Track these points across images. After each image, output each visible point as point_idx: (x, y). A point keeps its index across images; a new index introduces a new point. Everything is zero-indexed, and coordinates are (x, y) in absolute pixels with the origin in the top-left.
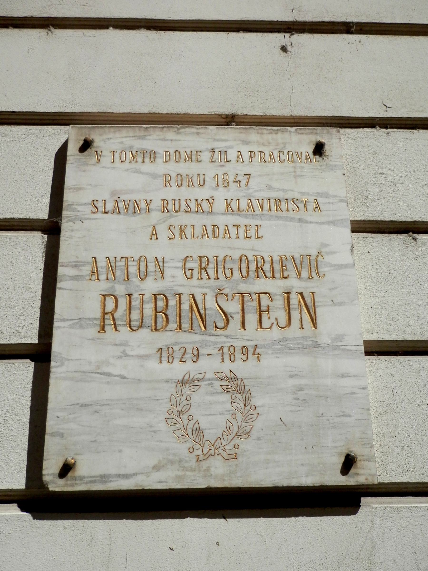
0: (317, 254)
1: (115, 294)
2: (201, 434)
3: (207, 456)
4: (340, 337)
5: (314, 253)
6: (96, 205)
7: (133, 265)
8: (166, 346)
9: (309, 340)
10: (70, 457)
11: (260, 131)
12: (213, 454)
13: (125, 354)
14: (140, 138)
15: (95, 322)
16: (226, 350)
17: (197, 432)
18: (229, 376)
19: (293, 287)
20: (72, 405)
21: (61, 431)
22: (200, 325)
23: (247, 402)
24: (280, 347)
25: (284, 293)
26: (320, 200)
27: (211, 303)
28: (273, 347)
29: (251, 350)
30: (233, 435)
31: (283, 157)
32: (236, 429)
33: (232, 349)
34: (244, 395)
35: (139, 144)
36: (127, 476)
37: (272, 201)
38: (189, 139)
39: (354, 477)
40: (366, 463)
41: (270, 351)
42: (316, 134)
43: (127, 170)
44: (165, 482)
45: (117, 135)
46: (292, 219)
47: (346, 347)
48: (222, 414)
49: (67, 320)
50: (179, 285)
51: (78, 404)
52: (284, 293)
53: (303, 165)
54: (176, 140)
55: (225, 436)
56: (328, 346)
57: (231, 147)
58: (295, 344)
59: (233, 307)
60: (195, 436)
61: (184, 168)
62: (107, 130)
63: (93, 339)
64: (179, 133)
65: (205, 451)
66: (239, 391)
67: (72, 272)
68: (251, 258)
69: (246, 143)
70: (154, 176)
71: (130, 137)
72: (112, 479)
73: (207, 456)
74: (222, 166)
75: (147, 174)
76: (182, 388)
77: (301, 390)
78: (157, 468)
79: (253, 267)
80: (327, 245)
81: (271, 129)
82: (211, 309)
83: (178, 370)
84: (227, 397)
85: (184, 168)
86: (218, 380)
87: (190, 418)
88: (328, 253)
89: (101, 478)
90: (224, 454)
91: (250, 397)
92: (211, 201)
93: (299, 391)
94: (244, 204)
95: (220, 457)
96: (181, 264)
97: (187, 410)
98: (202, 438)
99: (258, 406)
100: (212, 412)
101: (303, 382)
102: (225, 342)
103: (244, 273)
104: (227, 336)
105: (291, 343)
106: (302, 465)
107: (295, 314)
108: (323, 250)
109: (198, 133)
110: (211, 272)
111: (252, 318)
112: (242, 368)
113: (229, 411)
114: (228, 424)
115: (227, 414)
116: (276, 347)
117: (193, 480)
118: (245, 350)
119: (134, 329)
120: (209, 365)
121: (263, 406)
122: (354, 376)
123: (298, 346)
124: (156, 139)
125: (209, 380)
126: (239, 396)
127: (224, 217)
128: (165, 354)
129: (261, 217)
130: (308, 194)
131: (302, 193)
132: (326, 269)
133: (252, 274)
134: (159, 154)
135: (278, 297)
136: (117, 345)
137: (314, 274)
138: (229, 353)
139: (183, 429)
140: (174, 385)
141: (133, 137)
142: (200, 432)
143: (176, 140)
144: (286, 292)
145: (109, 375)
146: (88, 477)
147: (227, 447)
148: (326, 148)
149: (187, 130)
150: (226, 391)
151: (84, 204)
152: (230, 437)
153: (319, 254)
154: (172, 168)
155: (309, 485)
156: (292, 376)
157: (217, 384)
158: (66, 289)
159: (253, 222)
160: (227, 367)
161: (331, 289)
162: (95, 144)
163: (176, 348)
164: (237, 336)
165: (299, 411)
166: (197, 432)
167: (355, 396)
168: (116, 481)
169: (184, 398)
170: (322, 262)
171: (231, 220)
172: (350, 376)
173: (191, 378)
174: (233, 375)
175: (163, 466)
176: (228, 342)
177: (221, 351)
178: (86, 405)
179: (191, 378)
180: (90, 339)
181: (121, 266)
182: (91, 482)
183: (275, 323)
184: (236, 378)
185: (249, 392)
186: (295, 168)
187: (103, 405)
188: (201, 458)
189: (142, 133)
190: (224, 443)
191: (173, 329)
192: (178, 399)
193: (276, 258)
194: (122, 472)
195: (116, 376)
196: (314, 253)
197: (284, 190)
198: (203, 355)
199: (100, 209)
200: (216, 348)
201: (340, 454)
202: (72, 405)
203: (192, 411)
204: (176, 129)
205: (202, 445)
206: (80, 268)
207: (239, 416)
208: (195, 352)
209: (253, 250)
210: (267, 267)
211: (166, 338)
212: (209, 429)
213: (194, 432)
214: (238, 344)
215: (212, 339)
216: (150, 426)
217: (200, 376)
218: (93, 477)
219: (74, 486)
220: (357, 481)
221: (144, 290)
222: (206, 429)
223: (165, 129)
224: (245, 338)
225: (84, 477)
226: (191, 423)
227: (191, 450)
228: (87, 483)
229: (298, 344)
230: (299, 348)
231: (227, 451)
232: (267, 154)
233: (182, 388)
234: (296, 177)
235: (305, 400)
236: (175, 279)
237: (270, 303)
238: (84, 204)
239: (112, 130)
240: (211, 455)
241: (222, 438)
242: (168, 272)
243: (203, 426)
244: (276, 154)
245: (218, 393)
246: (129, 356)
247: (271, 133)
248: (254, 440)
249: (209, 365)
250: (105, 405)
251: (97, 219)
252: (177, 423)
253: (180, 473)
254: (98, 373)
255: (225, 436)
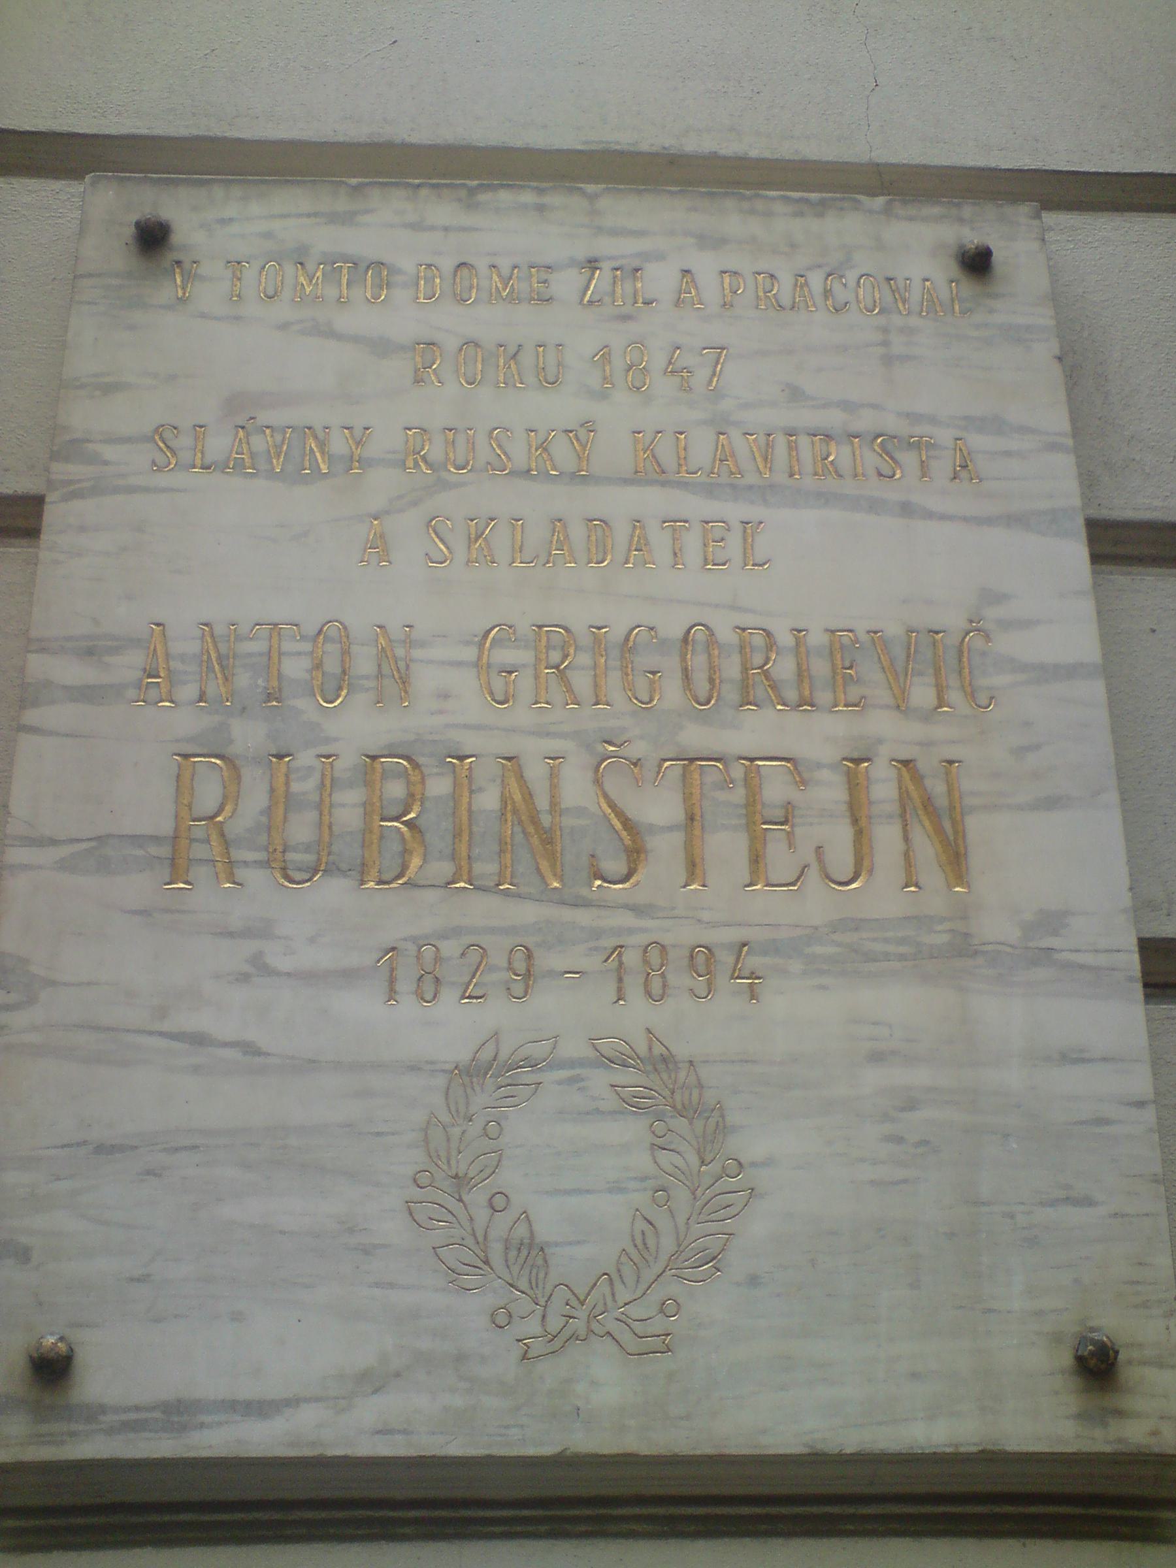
0: (967, 626)
1: (231, 751)
2: (540, 1262)
3: (559, 1342)
4: (1052, 921)
5: (953, 620)
6: (169, 444)
7: (299, 654)
8: (413, 939)
9: (939, 928)
10: (52, 1334)
11: (759, 205)
12: (582, 1333)
13: (261, 966)
14: (333, 218)
15: (153, 850)
16: (631, 958)
17: (525, 1252)
18: (642, 1049)
19: (880, 741)
20: (63, 1146)
21: (24, 1240)
22: (538, 870)
23: (709, 1147)
24: (831, 950)
25: (845, 759)
26: (978, 441)
27: (576, 789)
28: (808, 950)
29: (726, 959)
30: (657, 1269)
31: (841, 294)
32: (668, 1244)
33: (654, 956)
34: (699, 1124)
35: (325, 239)
36: (260, 1409)
37: (804, 441)
38: (511, 230)
39: (1105, 1425)
40: (1150, 1373)
41: (796, 966)
42: (961, 220)
43: (284, 327)
44: (405, 1432)
45: (255, 208)
46: (875, 506)
47: (1073, 957)
48: (616, 1188)
49: (54, 842)
50: (467, 727)
51: (85, 1143)
52: (845, 759)
53: (914, 321)
54: (463, 229)
55: (628, 1270)
56: (1009, 949)
57: (660, 257)
58: (886, 941)
59: (658, 808)
60: (515, 1269)
61: (487, 321)
62: (218, 192)
63: (144, 913)
64: (471, 206)
65: (554, 1323)
66: (679, 1107)
67: (70, 672)
68: (725, 634)
69: (708, 241)
70: (382, 347)
71: (299, 216)
72: (207, 1419)
73: (557, 1343)
74: (626, 318)
75: (356, 339)
76: (469, 1090)
77: (911, 1105)
78: (371, 1381)
79: (732, 668)
80: (998, 598)
81: (800, 200)
82: (581, 811)
83: (452, 1028)
84: (633, 1130)
85: (487, 321)
86: (603, 1065)
87: (499, 1201)
88: (1007, 625)
89: (164, 1412)
90: (626, 1338)
91: (723, 1129)
92: (582, 434)
93: (903, 1109)
94: (702, 449)
95: (609, 1346)
96: (470, 654)
97: (488, 1171)
98: (541, 1275)
99: (753, 1164)
100: (577, 1178)
101: (920, 1076)
102: (631, 931)
103: (701, 685)
104: (637, 910)
105: (874, 940)
106: (914, 1376)
107: (886, 837)
108: (992, 613)
109: (541, 208)
110: (581, 682)
111: (726, 846)
112: (701, 1026)
113: (644, 1179)
114: (641, 1225)
115: (637, 1190)
116: (818, 949)
117: (507, 1427)
118: (701, 960)
119: (298, 876)
120: (570, 1012)
121: (768, 1162)
122: (1104, 1059)
123: (902, 949)
124: (390, 227)
125: (572, 1063)
126: (680, 1124)
127: (632, 492)
128: (414, 971)
129: (765, 492)
130: (933, 420)
131: (914, 418)
132: (1000, 680)
133: (731, 694)
134: (399, 272)
135: (825, 775)
136: (231, 935)
137: (954, 696)
138: (645, 970)
139: (470, 1241)
140: (441, 1081)
141: (309, 215)
142: (534, 1253)
143: (463, 229)
144: (855, 755)
145: (199, 1040)
146: (117, 1410)
147: (636, 1311)
148: (997, 256)
149: (504, 196)
150: (632, 1105)
151: (127, 440)
152: (648, 1275)
153: (975, 625)
154: (450, 323)
155: (939, 1450)
156: (877, 1058)
157: (599, 1080)
158: (51, 733)
159: (735, 511)
160: (637, 1016)
161: (1020, 752)
162: (176, 238)
163: (450, 948)
164: (673, 908)
165: (905, 1181)
166: (525, 1252)
167: (1105, 1129)
168: (220, 1424)
169: (475, 1128)
170: (984, 654)
171: (653, 501)
172: (1090, 1061)
173: (503, 1056)
174: (658, 1049)
175: (398, 1375)
176: (644, 930)
177: (613, 962)
178: (113, 1146)
179: (503, 1056)
180: (129, 912)
181: (250, 655)
182: (127, 1427)
183: (815, 866)
184: (667, 1061)
185: (716, 1113)
186: (885, 330)
187: (177, 1150)
188: (538, 1347)
189: (342, 204)
190: (623, 1295)
191: (442, 881)
192: (456, 1132)
193: (817, 638)
194: (248, 1390)
195: (226, 1045)
196: (953, 620)
197: (847, 406)
198: (551, 974)
199: (185, 456)
200: (596, 949)
201: (1057, 1338)
202: (63, 1146)
203: (509, 1177)
204: (463, 193)
205: (542, 1302)
206: (107, 659)
207: (681, 1195)
208: (521, 966)
209: (734, 608)
210: (784, 668)
211: (409, 916)
212: (570, 1243)
213: (513, 1254)
214: (681, 935)
215: (583, 917)
216: (351, 1231)
217: (538, 1051)
218: (137, 1409)
219: (63, 1443)
220: (1120, 1440)
221: (336, 740)
222: (557, 1244)
223: (424, 192)
224: (706, 916)
225: (103, 1409)
226: (502, 1222)
227: (501, 1319)
228: (111, 1431)
229: (902, 941)
230: (902, 957)
231: (635, 1325)
232: (786, 280)
233: (469, 1090)
234: (888, 360)
235: (925, 1143)
236: (449, 702)
237: (794, 795)
238: (127, 440)
239: (236, 191)
240: (574, 1336)
241: (615, 1276)
242: (426, 680)
243: (545, 1231)
244: (816, 281)
245: (603, 1113)
246: (278, 974)
247: (801, 214)
248: (738, 1284)
249: (570, 1012)
250: (185, 1148)
251: (172, 490)
252: (450, 1218)
253: (458, 1401)
254: (161, 1034)
255: (628, 1270)
